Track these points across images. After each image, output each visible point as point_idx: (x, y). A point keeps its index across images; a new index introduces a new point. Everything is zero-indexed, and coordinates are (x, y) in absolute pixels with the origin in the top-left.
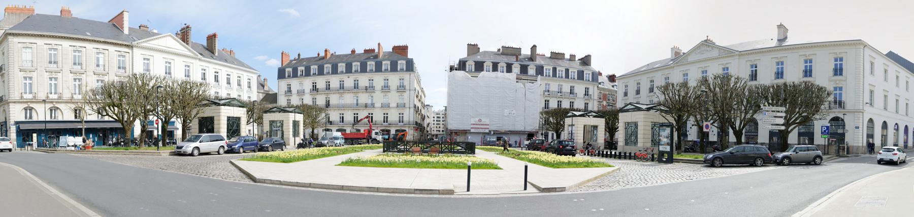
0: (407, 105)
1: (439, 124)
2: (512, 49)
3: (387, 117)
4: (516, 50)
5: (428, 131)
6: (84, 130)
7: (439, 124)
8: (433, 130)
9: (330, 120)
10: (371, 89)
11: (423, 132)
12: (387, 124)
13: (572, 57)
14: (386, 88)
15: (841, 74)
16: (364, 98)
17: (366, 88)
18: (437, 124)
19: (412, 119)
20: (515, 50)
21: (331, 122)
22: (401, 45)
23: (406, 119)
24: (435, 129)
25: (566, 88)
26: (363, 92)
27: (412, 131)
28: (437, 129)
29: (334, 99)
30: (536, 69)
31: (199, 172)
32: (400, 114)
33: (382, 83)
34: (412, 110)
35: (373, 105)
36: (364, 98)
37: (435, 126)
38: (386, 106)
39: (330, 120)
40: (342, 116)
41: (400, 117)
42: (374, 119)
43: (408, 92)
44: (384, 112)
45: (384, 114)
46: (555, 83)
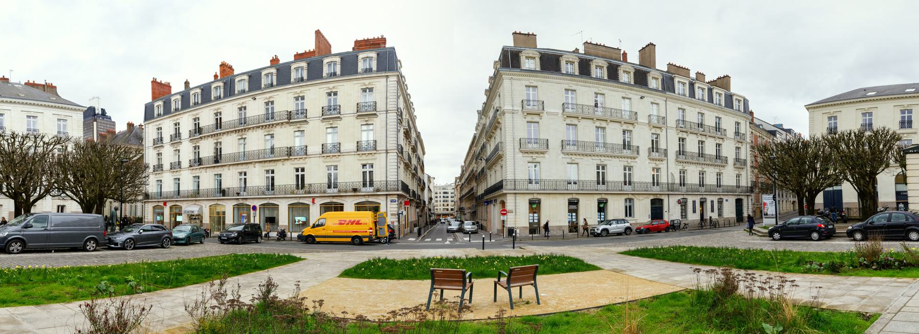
0: (381, 146)
1: (447, 201)
2: (604, 49)
3: (303, 176)
4: (611, 50)
5: (430, 210)
6: (332, 187)
7: (447, 201)
8: (437, 209)
9: (223, 187)
10: (300, 116)
11: (422, 210)
12: (371, 189)
13: (700, 76)
14: (331, 114)
15: (910, 126)
16: (285, 137)
17: (290, 115)
18: (444, 201)
19: (392, 177)
20: (608, 49)
21: (224, 191)
22: (376, 37)
23: (378, 178)
24: (442, 207)
25: (710, 121)
26: (282, 123)
27: (395, 205)
28: (444, 207)
29: (230, 145)
30: (663, 80)
31: (436, 193)
32: (364, 166)
33: (324, 102)
34: (393, 156)
35: (305, 151)
36: (285, 137)
37: (442, 203)
38: (332, 151)
39: (223, 187)
40: (270, 175)
41: (364, 173)
42: (307, 182)
43: (382, 117)
44: (297, 166)
45: (297, 170)
46: (693, 109)
